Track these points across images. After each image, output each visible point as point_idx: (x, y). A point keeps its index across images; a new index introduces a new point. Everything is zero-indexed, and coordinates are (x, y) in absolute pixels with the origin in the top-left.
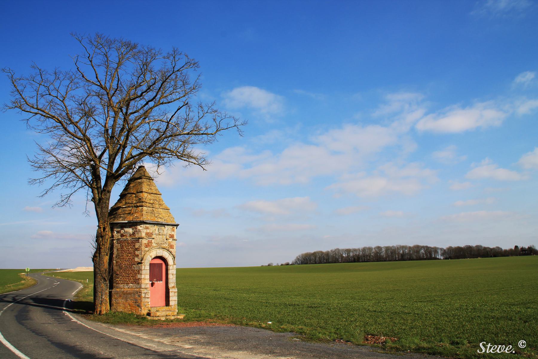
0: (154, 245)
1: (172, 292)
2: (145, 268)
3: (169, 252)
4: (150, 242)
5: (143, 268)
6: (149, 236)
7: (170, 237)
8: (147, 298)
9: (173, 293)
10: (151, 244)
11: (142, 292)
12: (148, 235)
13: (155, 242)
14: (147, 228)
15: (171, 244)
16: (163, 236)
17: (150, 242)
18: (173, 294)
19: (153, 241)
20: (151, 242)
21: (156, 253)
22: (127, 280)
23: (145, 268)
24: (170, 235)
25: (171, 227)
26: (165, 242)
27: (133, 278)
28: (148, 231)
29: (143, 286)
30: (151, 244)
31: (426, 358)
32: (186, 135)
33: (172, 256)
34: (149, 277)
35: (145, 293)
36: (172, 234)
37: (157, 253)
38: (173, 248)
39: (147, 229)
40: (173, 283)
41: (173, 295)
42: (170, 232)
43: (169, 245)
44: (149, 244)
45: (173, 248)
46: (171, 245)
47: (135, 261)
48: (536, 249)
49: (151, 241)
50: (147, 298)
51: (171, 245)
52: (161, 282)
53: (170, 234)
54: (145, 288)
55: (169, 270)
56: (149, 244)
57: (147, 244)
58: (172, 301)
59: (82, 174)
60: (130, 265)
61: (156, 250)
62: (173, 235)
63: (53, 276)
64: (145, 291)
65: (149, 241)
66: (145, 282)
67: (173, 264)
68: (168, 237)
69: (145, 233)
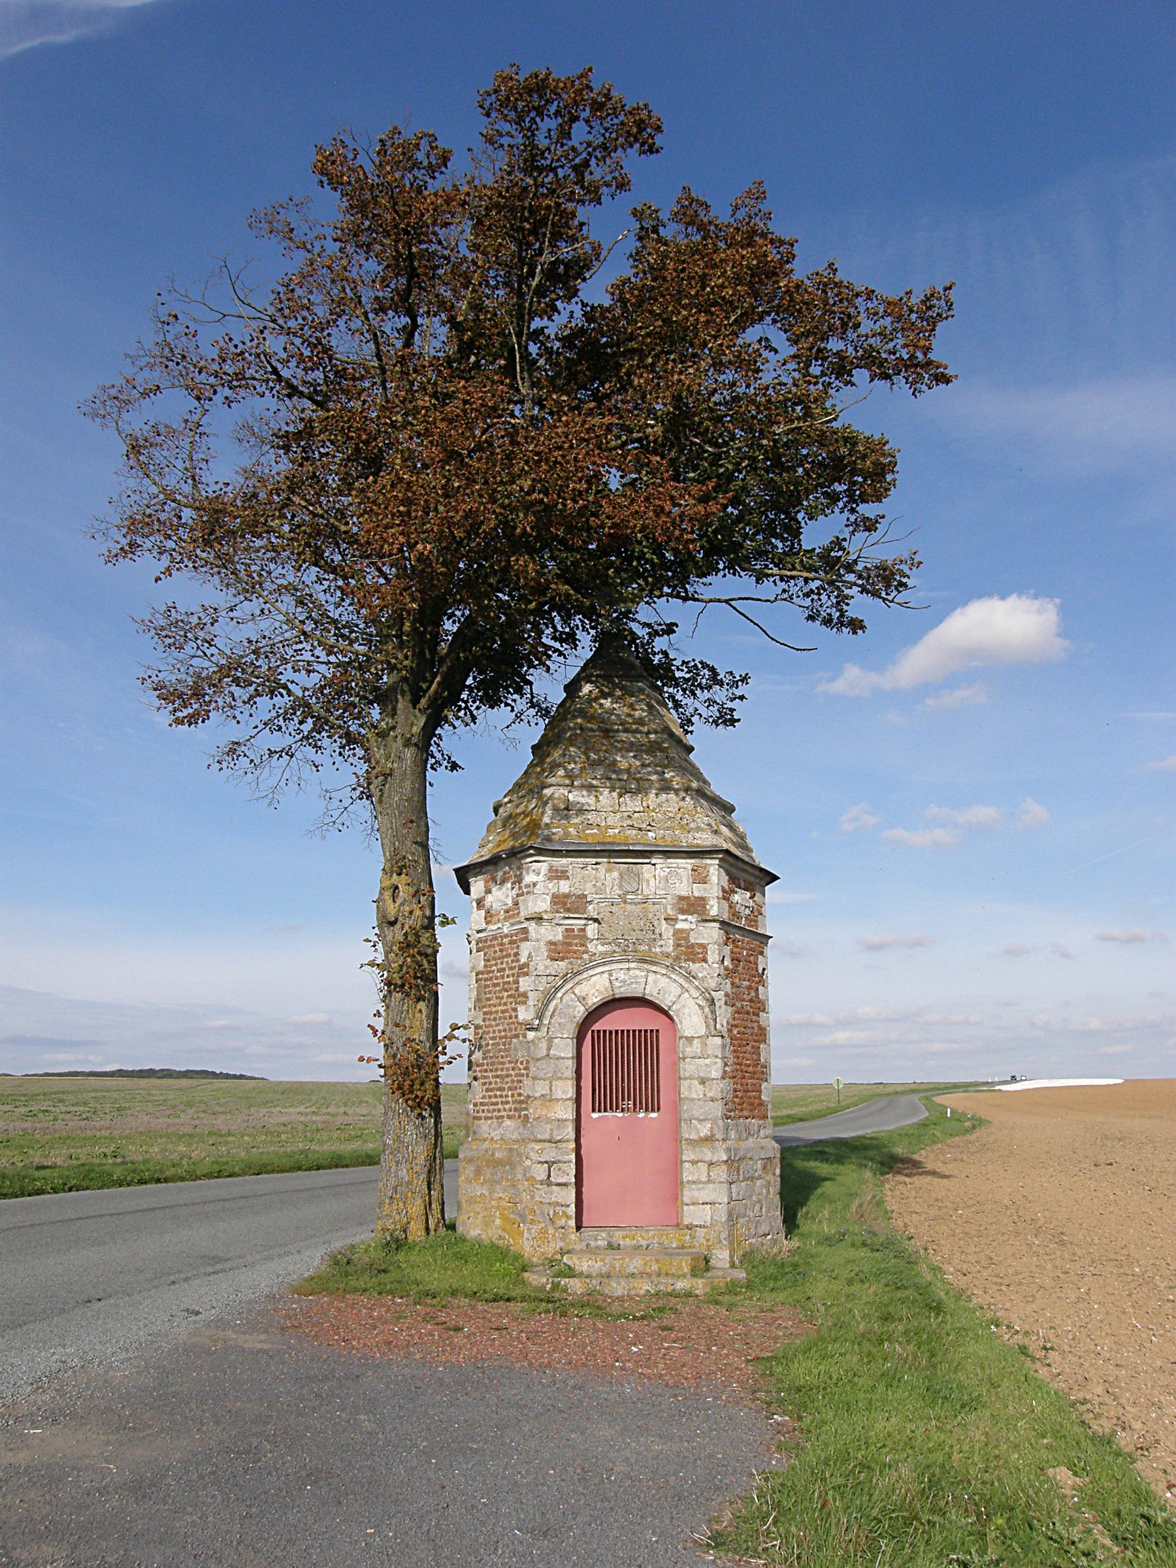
2: (549, 1049)
6: (568, 910)
7: (683, 911)
9: (703, 1167)
12: (565, 904)
14: (560, 875)
17: (575, 937)
19: (592, 929)
20: (585, 937)
21: (607, 984)
22: (497, 1104)
23: (549, 1049)
25: (688, 863)
27: (513, 1096)
28: (564, 887)
31: (1084, 1561)
37: (617, 984)
38: (705, 960)
39: (559, 878)
42: (683, 888)
43: (679, 945)
44: (570, 944)
45: (705, 960)
47: (518, 1023)
48: (1058, 615)
49: (584, 930)
51: (688, 947)
52: (654, 1115)
54: (550, 1141)
60: (505, 1037)
61: (606, 968)
62: (702, 899)
66: (551, 1115)
69: (548, 898)
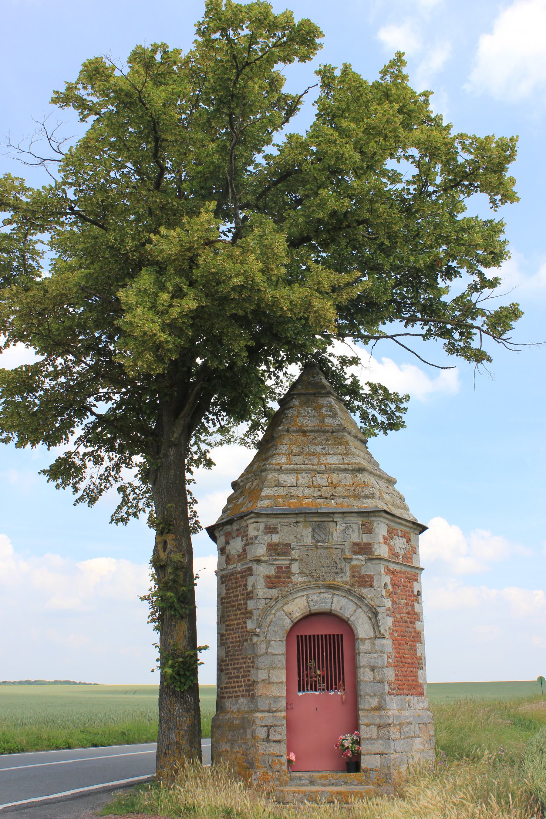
0: (298, 579)
1: (367, 725)
2: (267, 649)
3: (353, 599)
4: (283, 572)
5: (261, 650)
7: (356, 553)
8: (275, 741)
9: (374, 729)
10: (289, 578)
11: (258, 722)
13: (305, 571)
14: (271, 530)
15: (363, 573)
16: (334, 551)
18: (375, 733)
21: (305, 603)
23: (267, 649)
24: (355, 544)
26: (339, 567)
28: (275, 538)
29: (263, 704)
30: (289, 578)
32: (369, 469)
33: (366, 609)
34: (285, 650)
35: (269, 727)
36: (365, 541)
37: (312, 603)
38: (372, 586)
40: (375, 695)
41: (375, 737)
45: (372, 586)
46: (363, 577)
50: (275, 741)
53: (356, 541)
55: (359, 654)
56: (279, 577)
57: (273, 579)
58: (368, 754)
59: (302, 95)
63: (199, 361)
64: (268, 719)
65: (282, 568)
67: (372, 634)
68: (348, 554)
